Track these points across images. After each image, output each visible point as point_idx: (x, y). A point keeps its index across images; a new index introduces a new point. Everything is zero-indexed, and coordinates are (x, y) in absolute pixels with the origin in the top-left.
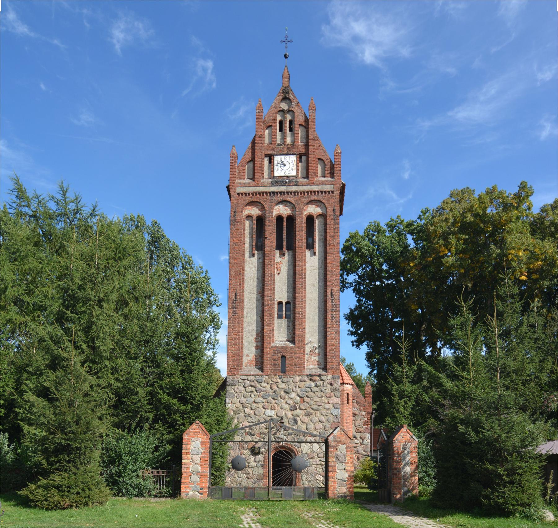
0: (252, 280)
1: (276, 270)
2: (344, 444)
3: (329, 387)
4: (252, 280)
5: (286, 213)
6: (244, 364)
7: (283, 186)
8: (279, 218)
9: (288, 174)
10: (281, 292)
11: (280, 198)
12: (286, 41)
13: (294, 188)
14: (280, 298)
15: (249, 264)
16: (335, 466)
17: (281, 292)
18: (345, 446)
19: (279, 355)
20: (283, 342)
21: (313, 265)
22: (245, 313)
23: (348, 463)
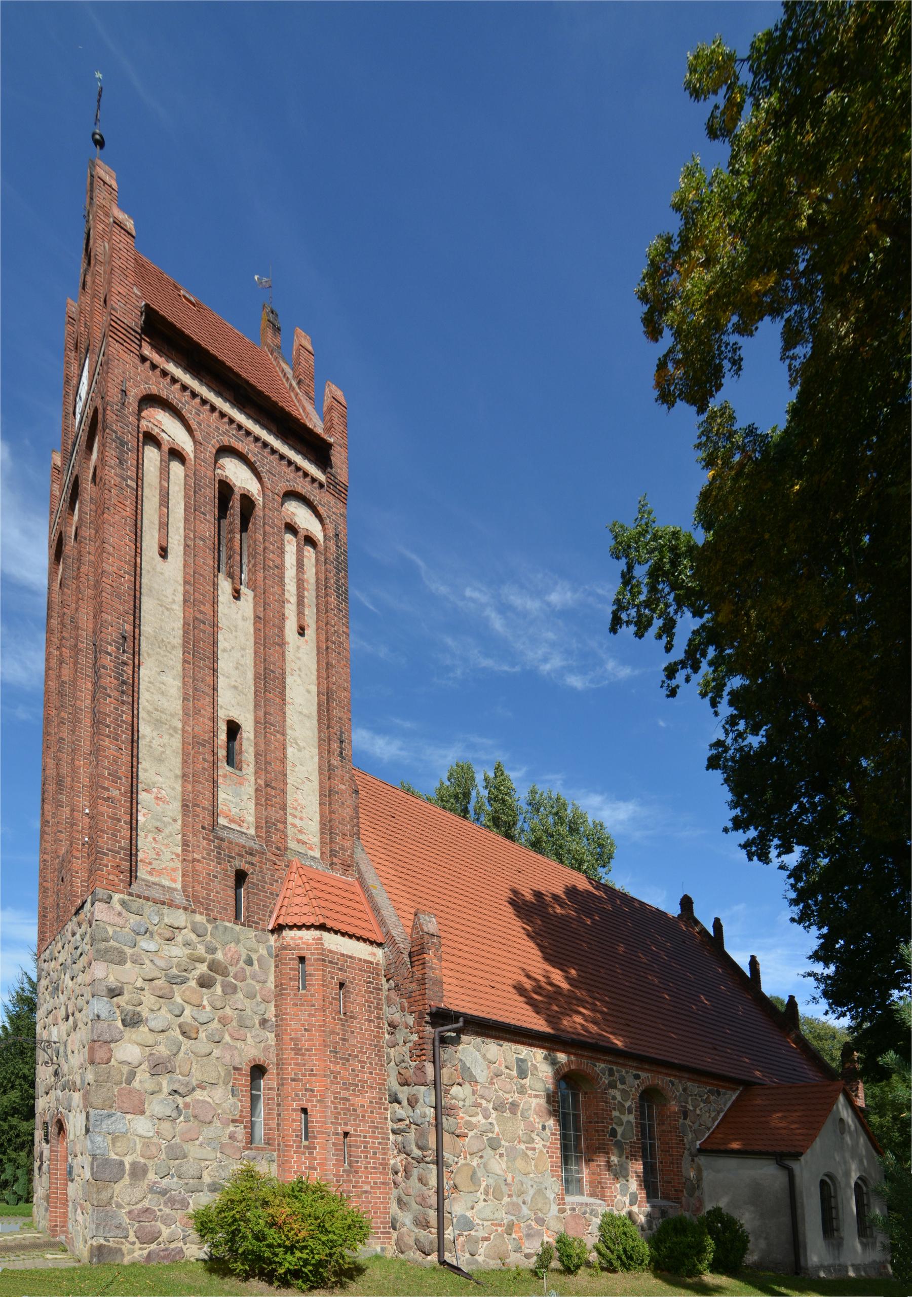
10: (235, 700)
17: (235, 700)
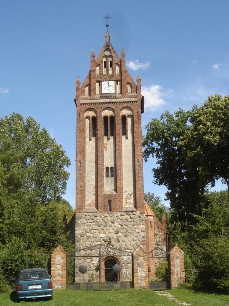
0: (90, 155)
1: (104, 148)
2: (142, 256)
3: (138, 219)
4: (90, 155)
5: (109, 115)
6: (86, 205)
7: (107, 99)
8: (106, 118)
9: (110, 92)
10: (108, 162)
11: (106, 106)
12: (107, 17)
13: (114, 100)
14: (107, 165)
15: (88, 145)
16: (137, 269)
18: (143, 257)
19: (107, 200)
20: (109, 191)
21: (126, 145)
22: (86, 174)
23: (145, 267)
